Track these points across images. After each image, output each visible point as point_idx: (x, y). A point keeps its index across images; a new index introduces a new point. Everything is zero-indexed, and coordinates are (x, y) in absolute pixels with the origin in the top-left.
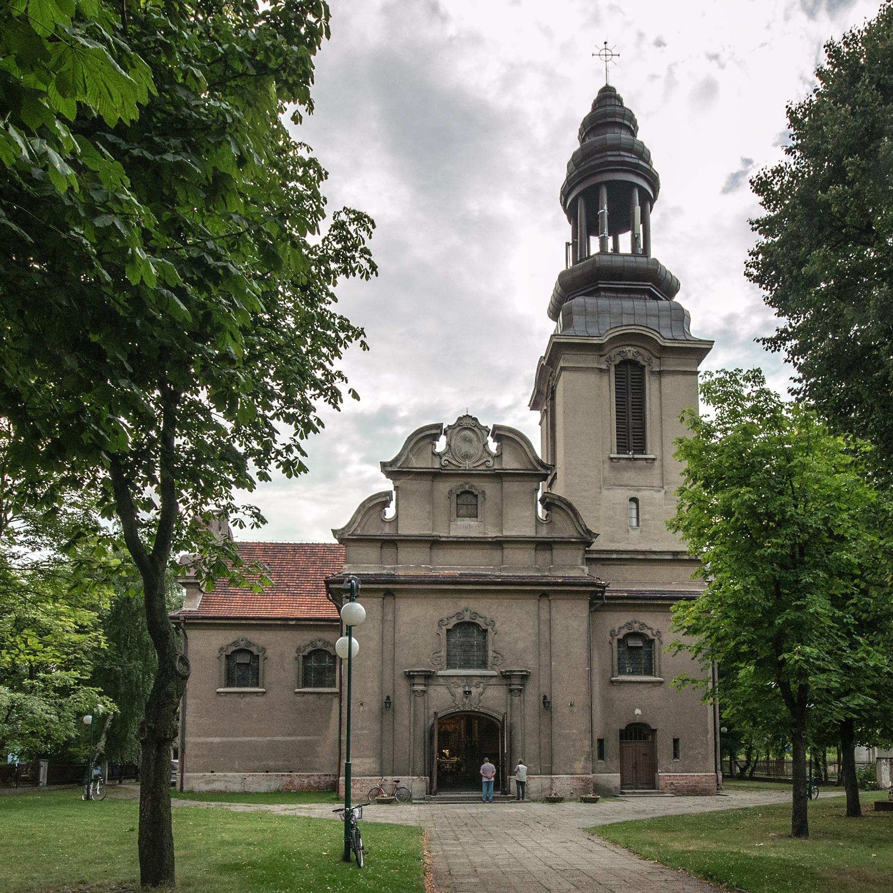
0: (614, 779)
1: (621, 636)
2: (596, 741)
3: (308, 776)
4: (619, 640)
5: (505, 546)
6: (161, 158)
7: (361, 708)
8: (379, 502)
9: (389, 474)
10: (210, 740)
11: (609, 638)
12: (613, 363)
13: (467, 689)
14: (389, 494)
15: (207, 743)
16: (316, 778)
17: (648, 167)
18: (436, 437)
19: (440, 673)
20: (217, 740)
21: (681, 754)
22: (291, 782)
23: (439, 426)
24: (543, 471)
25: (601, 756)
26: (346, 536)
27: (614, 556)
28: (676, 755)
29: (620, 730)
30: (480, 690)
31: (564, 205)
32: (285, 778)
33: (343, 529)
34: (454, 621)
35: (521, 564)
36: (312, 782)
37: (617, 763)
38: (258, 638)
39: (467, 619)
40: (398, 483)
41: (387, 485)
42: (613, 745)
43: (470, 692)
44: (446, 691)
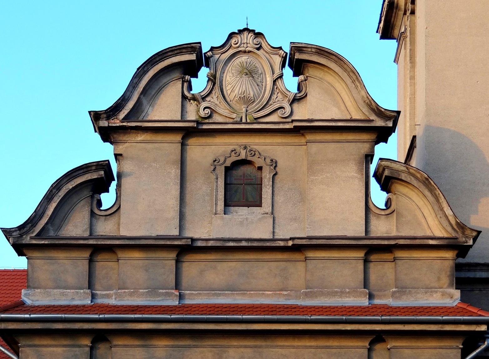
5: (311, 254)
8: (91, 181)
14: (105, 166)
18: (191, 69)
23: (195, 48)
24: (379, 123)
40: (121, 149)
41: (104, 152)
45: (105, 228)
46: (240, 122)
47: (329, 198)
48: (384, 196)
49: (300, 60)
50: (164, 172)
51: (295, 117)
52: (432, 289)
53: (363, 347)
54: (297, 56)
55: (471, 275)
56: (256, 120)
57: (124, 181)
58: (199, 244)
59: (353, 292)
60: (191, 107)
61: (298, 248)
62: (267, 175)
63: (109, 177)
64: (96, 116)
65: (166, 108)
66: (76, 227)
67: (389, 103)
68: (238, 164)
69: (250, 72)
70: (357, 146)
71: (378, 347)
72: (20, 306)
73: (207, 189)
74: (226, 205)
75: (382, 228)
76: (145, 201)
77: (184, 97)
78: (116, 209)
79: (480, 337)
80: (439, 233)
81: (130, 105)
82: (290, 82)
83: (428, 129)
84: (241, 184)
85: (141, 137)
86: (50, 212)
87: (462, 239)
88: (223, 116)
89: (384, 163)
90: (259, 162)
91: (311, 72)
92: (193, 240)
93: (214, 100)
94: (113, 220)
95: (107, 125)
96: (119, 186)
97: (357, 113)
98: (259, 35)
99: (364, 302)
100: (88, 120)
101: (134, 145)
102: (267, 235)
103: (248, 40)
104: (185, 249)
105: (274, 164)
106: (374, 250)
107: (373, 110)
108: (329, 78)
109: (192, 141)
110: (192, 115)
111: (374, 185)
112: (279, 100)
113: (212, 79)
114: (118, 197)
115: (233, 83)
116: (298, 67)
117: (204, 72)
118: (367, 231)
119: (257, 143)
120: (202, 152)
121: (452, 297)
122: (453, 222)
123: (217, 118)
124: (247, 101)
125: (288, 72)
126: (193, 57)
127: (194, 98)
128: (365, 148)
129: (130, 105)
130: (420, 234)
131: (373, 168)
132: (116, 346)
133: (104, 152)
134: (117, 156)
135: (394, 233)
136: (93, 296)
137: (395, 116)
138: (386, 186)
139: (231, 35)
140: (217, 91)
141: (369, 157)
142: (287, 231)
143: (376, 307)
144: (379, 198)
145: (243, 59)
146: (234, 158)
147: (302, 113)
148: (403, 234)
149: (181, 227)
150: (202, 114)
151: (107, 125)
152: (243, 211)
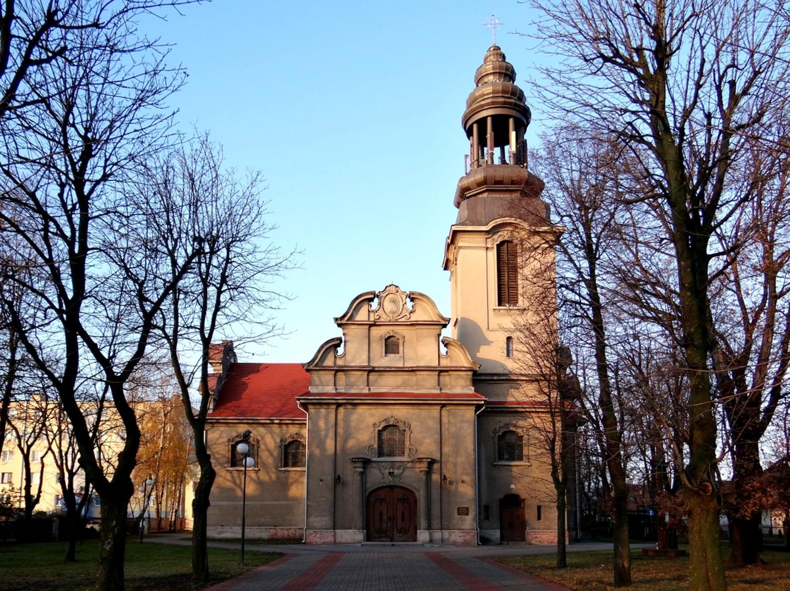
0: (496, 534)
1: (500, 434)
2: (483, 507)
3: (287, 530)
4: (499, 436)
6: (91, 431)
7: (321, 483)
8: (333, 345)
9: (339, 325)
10: (220, 503)
11: (492, 435)
12: (496, 243)
13: (391, 471)
14: (340, 339)
15: (218, 505)
16: (293, 531)
17: (522, 104)
18: (372, 300)
19: (374, 459)
20: (225, 503)
21: (542, 517)
22: (276, 534)
23: (373, 293)
24: (443, 323)
25: (487, 518)
26: (311, 367)
27: (495, 378)
28: (539, 518)
29: (500, 499)
30: (401, 471)
31: (465, 128)
32: (271, 531)
33: (309, 363)
34: (383, 425)
35: (427, 385)
36: (290, 534)
37: (497, 523)
38: (400, 413)
39: (391, 423)
40: (345, 331)
41: (338, 332)
42: (495, 509)
43: (393, 473)
44: (378, 472)
45: (340, 362)
46: (390, 321)
47: (423, 351)
48: (445, 349)
49: (412, 297)
50: (126, 236)
51: (411, 320)
52: (461, 386)
53: (214, 540)
54: (412, 296)
55: (479, 378)
56: (396, 320)
57: (347, 344)
58: (376, 369)
59: (434, 388)
60: (372, 315)
61: (413, 370)
62: (401, 342)
63: (341, 341)
64: (336, 319)
65: (362, 315)
66: (329, 362)
67: (446, 315)
68: (389, 337)
69: (394, 301)
70: (434, 330)
71: (444, 409)
72: (308, 394)
73: (378, 348)
74: (386, 353)
75: (445, 363)
76: (354, 353)
77: (369, 311)
78: (344, 355)
79: (481, 406)
80: (466, 365)
81: (349, 315)
82: (409, 304)
83: (462, 318)
84: (391, 345)
85: (353, 327)
86: (319, 357)
87: (474, 368)
88: (384, 319)
90: (397, 336)
91: (417, 301)
92: (374, 368)
93: (381, 312)
94: (343, 359)
95: (341, 322)
96: (345, 345)
97: (435, 318)
98: (397, 287)
99: (438, 392)
100: (333, 321)
101: (353, 330)
102: (401, 365)
103: (393, 289)
104: (371, 370)
105: (404, 337)
106: (441, 371)
108: (424, 304)
109: (372, 328)
110: (372, 319)
111: (442, 345)
112: (405, 313)
113: (380, 304)
114: (345, 350)
115: (388, 306)
116: (412, 300)
117: (376, 300)
118: (439, 364)
119: (395, 328)
120: (376, 332)
121: (471, 390)
123: (382, 319)
124: (393, 313)
125: (408, 300)
126: (372, 296)
127: (373, 311)
128: (437, 332)
129: (349, 315)
130: (459, 365)
131: (441, 338)
133: (338, 332)
134: (344, 334)
135: (449, 365)
136: (336, 389)
137: (449, 320)
138: (446, 346)
139: (386, 287)
140: (381, 309)
141: (439, 335)
142: (409, 364)
143: (442, 394)
144: (443, 350)
145: (391, 296)
146: (388, 335)
147: (414, 318)
148: (452, 365)
149: (369, 362)
150: (376, 317)
151: (341, 322)
152: (392, 355)
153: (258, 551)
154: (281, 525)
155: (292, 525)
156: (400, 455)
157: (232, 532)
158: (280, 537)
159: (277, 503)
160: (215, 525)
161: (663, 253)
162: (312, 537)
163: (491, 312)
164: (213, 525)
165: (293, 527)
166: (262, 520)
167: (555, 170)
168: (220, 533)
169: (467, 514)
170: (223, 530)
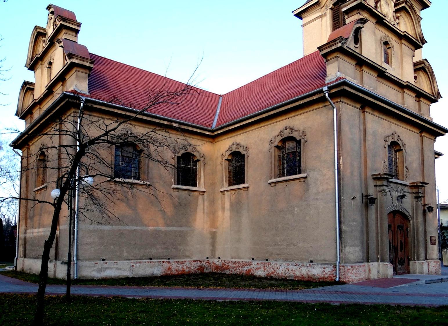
3: (182, 263)
10: (101, 227)
16: (188, 264)
22: (170, 268)
34: (182, 152)
36: (185, 267)
89: (425, 61)
107: (420, 38)
122: (436, 91)
132: (367, 112)
153: (101, 296)
154: (175, 257)
155: (187, 257)
156: (403, 273)
157: (118, 269)
158: (174, 272)
159: (171, 228)
160: (94, 259)
161: (339, 295)
162: (349, 274)
163: (378, 192)
164: (90, 260)
165: (187, 260)
166: (154, 251)
167: (358, 272)
168: (100, 270)
169: (435, 244)
170: (105, 266)
